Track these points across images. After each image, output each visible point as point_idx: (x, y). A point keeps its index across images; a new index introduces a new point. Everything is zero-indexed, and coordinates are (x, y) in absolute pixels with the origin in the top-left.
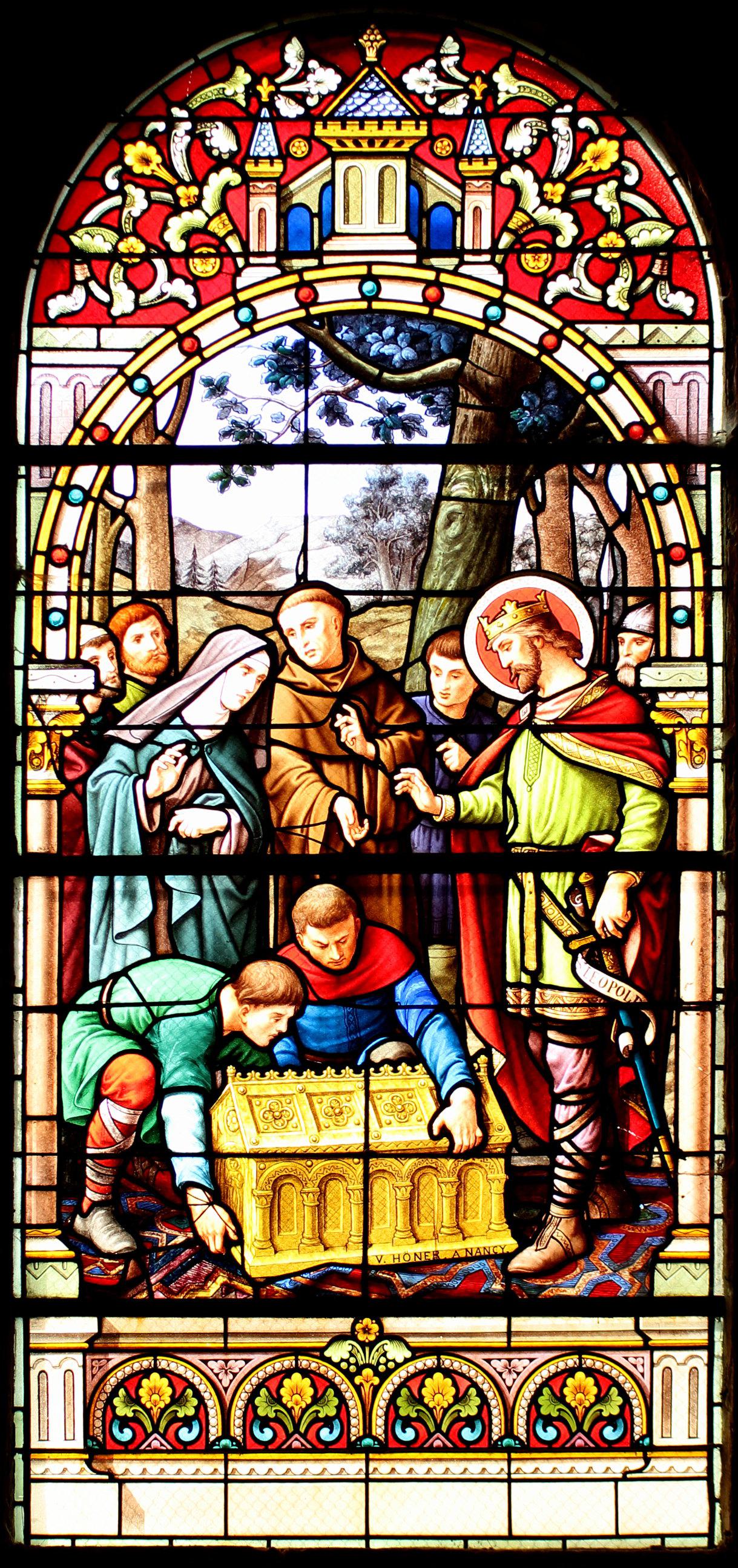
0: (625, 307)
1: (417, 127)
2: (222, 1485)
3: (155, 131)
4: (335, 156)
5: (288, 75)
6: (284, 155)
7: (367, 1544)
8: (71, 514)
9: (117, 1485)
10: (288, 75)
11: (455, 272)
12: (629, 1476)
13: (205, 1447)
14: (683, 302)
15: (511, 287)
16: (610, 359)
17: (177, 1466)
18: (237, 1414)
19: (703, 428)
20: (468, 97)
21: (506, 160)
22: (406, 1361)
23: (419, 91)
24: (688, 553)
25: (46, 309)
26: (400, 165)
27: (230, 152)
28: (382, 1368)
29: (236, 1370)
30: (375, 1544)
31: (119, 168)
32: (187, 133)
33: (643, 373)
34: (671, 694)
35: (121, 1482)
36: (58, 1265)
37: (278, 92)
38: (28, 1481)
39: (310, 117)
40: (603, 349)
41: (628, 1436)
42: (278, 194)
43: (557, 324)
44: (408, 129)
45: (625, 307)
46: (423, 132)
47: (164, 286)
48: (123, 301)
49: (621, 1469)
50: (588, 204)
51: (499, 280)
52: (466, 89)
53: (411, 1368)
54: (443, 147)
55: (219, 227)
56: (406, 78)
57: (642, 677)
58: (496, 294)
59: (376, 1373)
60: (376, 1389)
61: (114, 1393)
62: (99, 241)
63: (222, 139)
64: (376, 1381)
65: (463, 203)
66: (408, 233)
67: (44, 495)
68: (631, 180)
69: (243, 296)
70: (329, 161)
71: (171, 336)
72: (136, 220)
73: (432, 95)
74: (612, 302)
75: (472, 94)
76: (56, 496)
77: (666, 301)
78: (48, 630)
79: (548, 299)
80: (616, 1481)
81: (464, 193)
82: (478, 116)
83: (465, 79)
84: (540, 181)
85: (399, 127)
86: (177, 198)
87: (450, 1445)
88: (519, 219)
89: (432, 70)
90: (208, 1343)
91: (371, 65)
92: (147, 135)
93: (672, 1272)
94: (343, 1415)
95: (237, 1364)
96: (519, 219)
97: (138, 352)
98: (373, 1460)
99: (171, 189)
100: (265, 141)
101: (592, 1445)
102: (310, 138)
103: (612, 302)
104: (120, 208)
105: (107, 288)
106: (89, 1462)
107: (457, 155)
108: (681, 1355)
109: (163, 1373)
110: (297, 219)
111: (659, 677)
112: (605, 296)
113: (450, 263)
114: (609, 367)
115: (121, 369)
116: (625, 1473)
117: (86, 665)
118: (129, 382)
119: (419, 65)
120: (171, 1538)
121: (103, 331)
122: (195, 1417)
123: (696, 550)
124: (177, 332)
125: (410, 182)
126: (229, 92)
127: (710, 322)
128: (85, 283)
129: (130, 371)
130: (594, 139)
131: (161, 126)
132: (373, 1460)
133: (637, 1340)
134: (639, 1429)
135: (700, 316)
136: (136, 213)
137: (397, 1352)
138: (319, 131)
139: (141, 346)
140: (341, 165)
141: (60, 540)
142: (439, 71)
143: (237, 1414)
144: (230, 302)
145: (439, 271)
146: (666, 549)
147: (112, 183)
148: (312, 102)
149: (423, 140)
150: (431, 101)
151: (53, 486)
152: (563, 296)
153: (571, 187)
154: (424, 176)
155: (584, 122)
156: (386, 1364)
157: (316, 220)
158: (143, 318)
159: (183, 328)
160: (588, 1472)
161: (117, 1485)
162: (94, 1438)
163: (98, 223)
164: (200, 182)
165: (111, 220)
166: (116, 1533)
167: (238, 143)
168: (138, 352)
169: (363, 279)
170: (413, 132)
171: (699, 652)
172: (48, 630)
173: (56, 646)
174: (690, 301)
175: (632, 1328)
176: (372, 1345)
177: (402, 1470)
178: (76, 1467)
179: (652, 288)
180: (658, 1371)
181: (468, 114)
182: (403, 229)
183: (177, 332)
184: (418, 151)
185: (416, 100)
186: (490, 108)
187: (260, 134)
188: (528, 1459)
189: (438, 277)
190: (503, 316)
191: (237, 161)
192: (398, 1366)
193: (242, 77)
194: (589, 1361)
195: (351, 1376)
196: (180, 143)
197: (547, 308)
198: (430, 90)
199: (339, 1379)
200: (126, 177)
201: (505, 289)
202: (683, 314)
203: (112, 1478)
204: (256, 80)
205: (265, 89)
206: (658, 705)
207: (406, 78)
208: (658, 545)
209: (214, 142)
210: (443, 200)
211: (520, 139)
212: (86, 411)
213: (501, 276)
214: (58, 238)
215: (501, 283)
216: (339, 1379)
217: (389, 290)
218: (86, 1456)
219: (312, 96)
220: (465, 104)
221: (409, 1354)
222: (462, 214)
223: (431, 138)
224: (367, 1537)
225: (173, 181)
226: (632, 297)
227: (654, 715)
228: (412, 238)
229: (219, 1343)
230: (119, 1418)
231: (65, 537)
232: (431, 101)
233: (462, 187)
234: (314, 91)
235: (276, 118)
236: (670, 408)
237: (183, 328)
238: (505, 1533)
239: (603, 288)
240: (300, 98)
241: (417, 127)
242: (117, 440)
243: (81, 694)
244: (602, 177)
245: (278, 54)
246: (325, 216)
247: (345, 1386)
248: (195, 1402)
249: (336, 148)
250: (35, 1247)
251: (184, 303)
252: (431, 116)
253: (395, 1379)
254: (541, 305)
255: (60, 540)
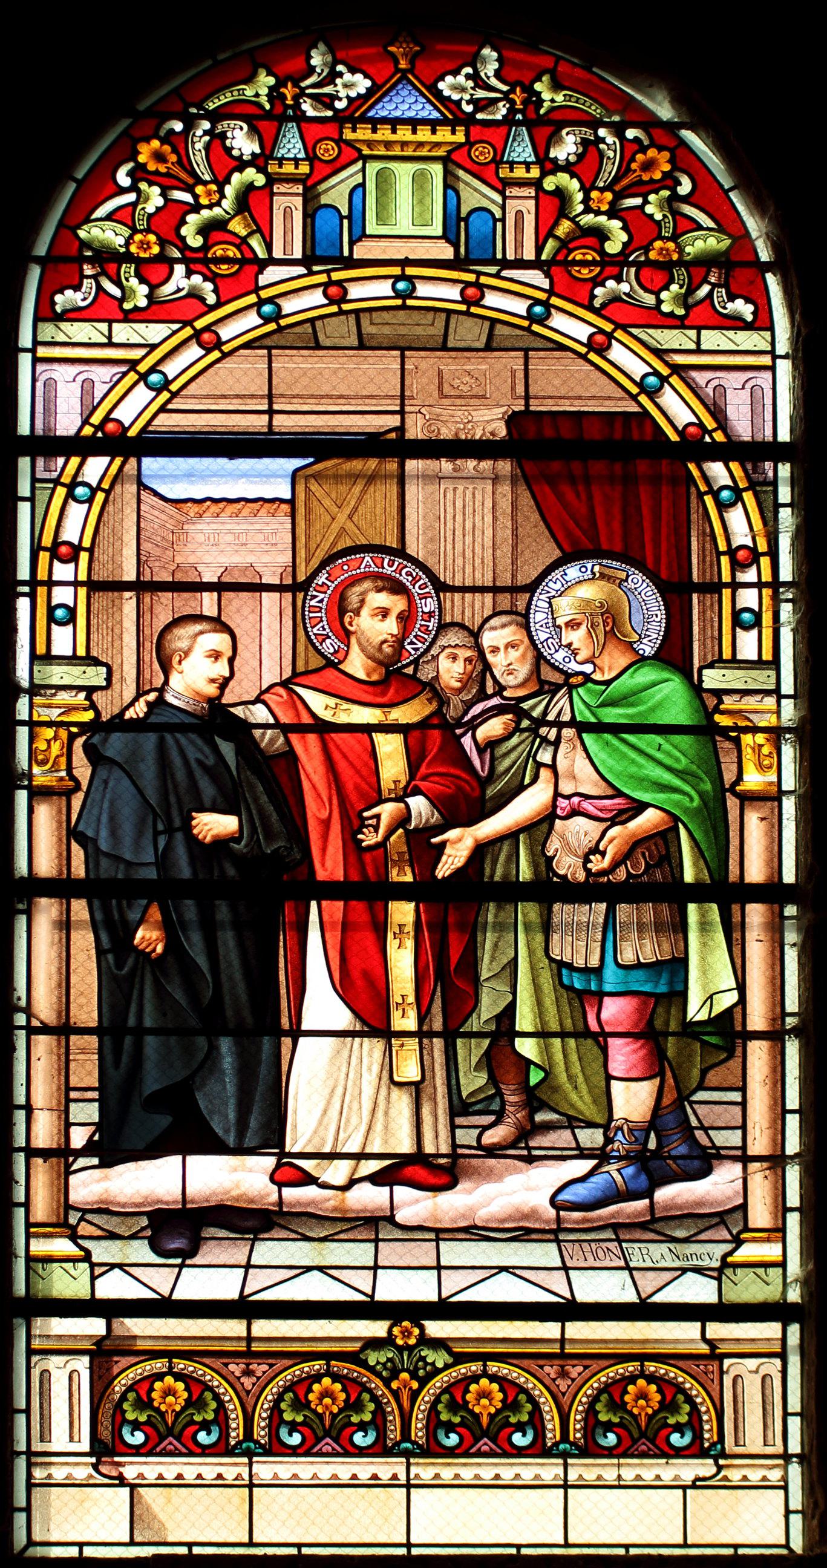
0: (680, 312)
1: (453, 132)
2: (562, 1491)
3: (172, 131)
4: (366, 159)
5: (313, 79)
6: (311, 158)
7: (409, 1551)
8: (77, 512)
9: (128, 1489)
10: (313, 79)
11: (497, 276)
12: (698, 1483)
13: (539, 1450)
14: (743, 308)
15: (556, 290)
16: (666, 363)
17: (517, 1470)
18: (261, 1415)
19: (769, 432)
20: (508, 106)
21: (550, 166)
22: (447, 1367)
23: (456, 97)
24: (755, 556)
25: (54, 303)
26: (437, 169)
27: (253, 154)
28: (421, 1373)
29: (259, 1374)
30: (415, 1551)
31: (131, 165)
32: (206, 133)
33: (700, 378)
34: (759, 697)
35: (133, 1487)
36: (68, 1266)
37: (302, 93)
38: (30, 1486)
39: (341, 119)
40: (659, 353)
41: (223, 1442)
42: (304, 195)
43: (608, 327)
44: (444, 135)
45: (680, 312)
46: (460, 137)
47: (179, 280)
48: (140, 295)
49: (692, 1478)
50: (639, 211)
51: (546, 284)
52: (506, 97)
53: (455, 1373)
54: (483, 153)
55: (237, 227)
56: (441, 85)
57: (704, 678)
58: (542, 296)
59: (414, 1375)
60: (414, 1395)
61: (123, 1398)
62: (113, 236)
63: (243, 143)
64: (415, 1385)
65: (503, 208)
66: (445, 237)
67: (51, 485)
68: (685, 187)
69: (264, 294)
70: (360, 164)
71: (188, 331)
72: (150, 216)
73: (468, 102)
74: (666, 308)
75: (512, 102)
76: (61, 492)
77: (127, 279)
78: (54, 626)
79: (597, 303)
80: (684, 1488)
81: (505, 198)
82: (519, 123)
83: (505, 88)
84: (586, 190)
85: (434, 132)
86: (196, 197)
87: (339, 1449)
88: (564, 228)
89: (468, 77)
90: (229, 1347)
91: (404, 72)
92: (162, 133)
93: (79, 1271)
94: (221, 1417)
95: (260, 1369)
96: (564, 228)
97: (153, 347)
98: (572, 1465)
99: (190, 189)
100: (291, 145)
101: (499, 1451)
102: (339, 141)
103: (666, 308)
104: (134, 205)
105: (118, 283)
106: (95, 1467)
107: (497, 161)
108: (752, 1363)
109: (493, 1378)
110: (325, 221)
111: (723, 679)
112: (660, 302)
113: (493, 270)
114: (665, 371)
115: (133, 364)
116: (694, 1482)
117: (97, 662)
118: (143, 377)
119: (456, 73)
120: (736, 1547)
121: (115, 326)
122: (214, 1421)
123: (764, 554)
124: (193, 328)
125: (446, 186)
126: (249, 92)
127: (771, 328)
128: (95, 277)
129: (142, 368)
130: (644, 150)
131: (178, 126)
132: (572, 1465)
133: (704, 1349)
134: (709, 1435)
135: (763, 322)
136: (150, 208)
137: (439, 1359)
138: (348, 135)
139: (156, 341)
140: (373, 168)
141: (65, 536)
142: (475, 77)
143: (261, 1415)
144: (252, 299)
145: (479, 274)
146: (732, 552)
147: (123, 179)
148: (340, 105)
149: (460, 146)
150: (469, 109)
151: (57, 482)
152: (615, 299)
153: (619, 196)
154: (458, 178)
155: (631, 133)
156: (424, 1369)
157: (346, 222)
158: (161, 312)
159: (199, 324)
160: (236, 1479)
161: (128, 1489)
162: (101, 1442)
163: (109, 217)
164: (222, 182)
165: (124, 215)
166: (127, 1539)
167: (261, 146)
168: (153, 347)
169: (397, 279)
170: (451, 138)
171: (767, 656)
172: (54, 626)
173: (62, 641)
174: (750, 308)
175: (698, 1336)
176: (410, 1349)
177: (447, 1474)
178: (82, 1472)
179: (710, 295)
180: (728, 1381)
181: (508, 121)
182: (439, 233)
183: (193, 328)
184: (454, 157)
185: (452, 106)
186: (532, 115)
187: (284, 136)
188: (265, 1462)
189: (478, 278)
190: (279, 307)
191: (259, 162)
192: (438, 1371)
193: (264, 80)
194: (651, 1367)
195: (387, 1383)
196: (199, 144)
197: (596, 312)
198: (467, 97)
199: (376, 1383)
200: (139, 174)
201: (551, 292)
202: (744, 321)
203: (122, 1481)
204: (280, 83)
205: (289, 92)
206: (722, 707)
207: (441, 85)
208: (722, 547)
209: (236, 144)
210: (484, 205)
211: (566, 148)
212: (95, 409)
213: (547, 280)
214: (67, 233)
215: (547, 287)
216: (376, 1383)
217: (289, 306)
218: (93, 1460)
219: (340, 99)
220: (504, 111)
221: (450, 1360)
222: (503, 220)
223: (469, 143)
224: (409, 1545)
225: (191, 181)
226: (683, 300)
227: (717, 718)
228: (448, 241)
229: (242, 1347)
230: (287, 1423)
231: (71, 533)
232: (469, 109)
233: (502, 193)
234: (343, 93)
235: (300, 118)
236: (731, 412)
237: (199, 324)
238: (246, 1540)
239: (657, 294)
240: (327, 101)
241: (453, 132)
242: (132, 433)
243: (90, 690)
244: (655, 187)
245: (303, 58)
246: (355, 219)
247: (381, 1390)
248: (529, 1407)
249: (366, 151)
250: (39, 1247)
251: (203, 300)
252: (468, 121)
253: (438, 1383)
254: (590, 308)
255: (65, 536)
